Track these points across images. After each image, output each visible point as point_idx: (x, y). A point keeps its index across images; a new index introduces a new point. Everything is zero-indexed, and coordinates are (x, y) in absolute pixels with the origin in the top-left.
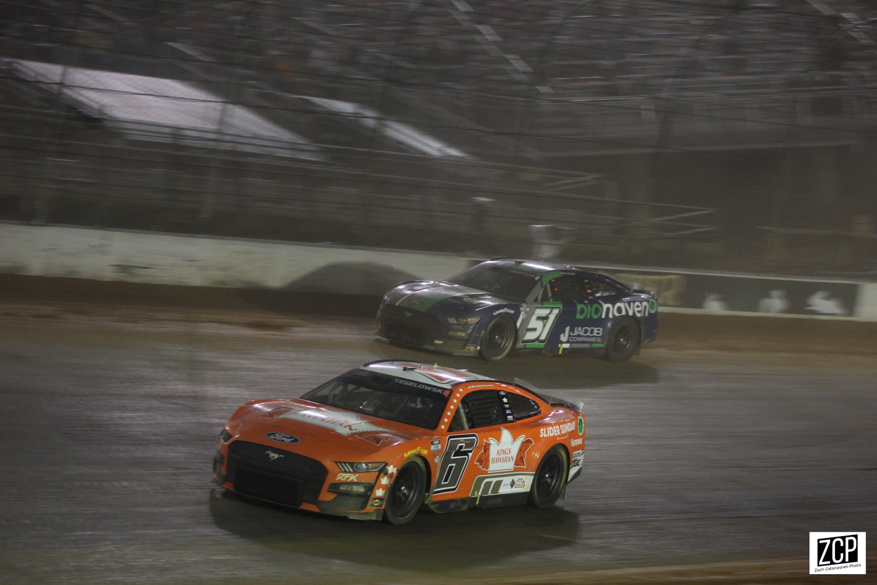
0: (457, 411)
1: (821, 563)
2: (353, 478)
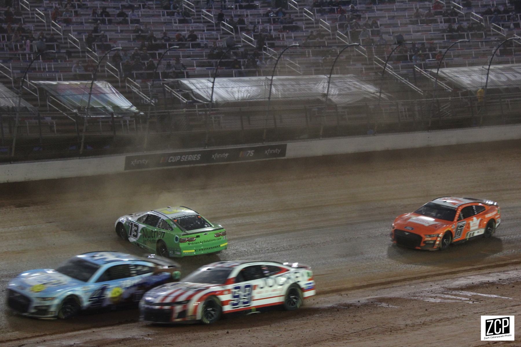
0: (460, 215)
1: (488, 334)
2: (430, 239)
